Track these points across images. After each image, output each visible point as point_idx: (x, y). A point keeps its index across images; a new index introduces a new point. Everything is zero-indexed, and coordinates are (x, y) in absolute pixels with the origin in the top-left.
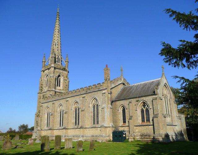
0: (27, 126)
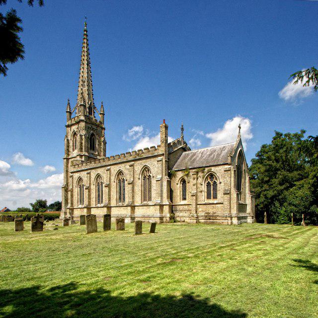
0: (45, 202)
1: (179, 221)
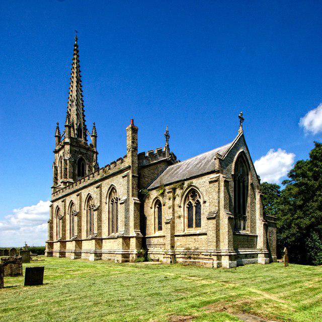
1: (152, 260)
